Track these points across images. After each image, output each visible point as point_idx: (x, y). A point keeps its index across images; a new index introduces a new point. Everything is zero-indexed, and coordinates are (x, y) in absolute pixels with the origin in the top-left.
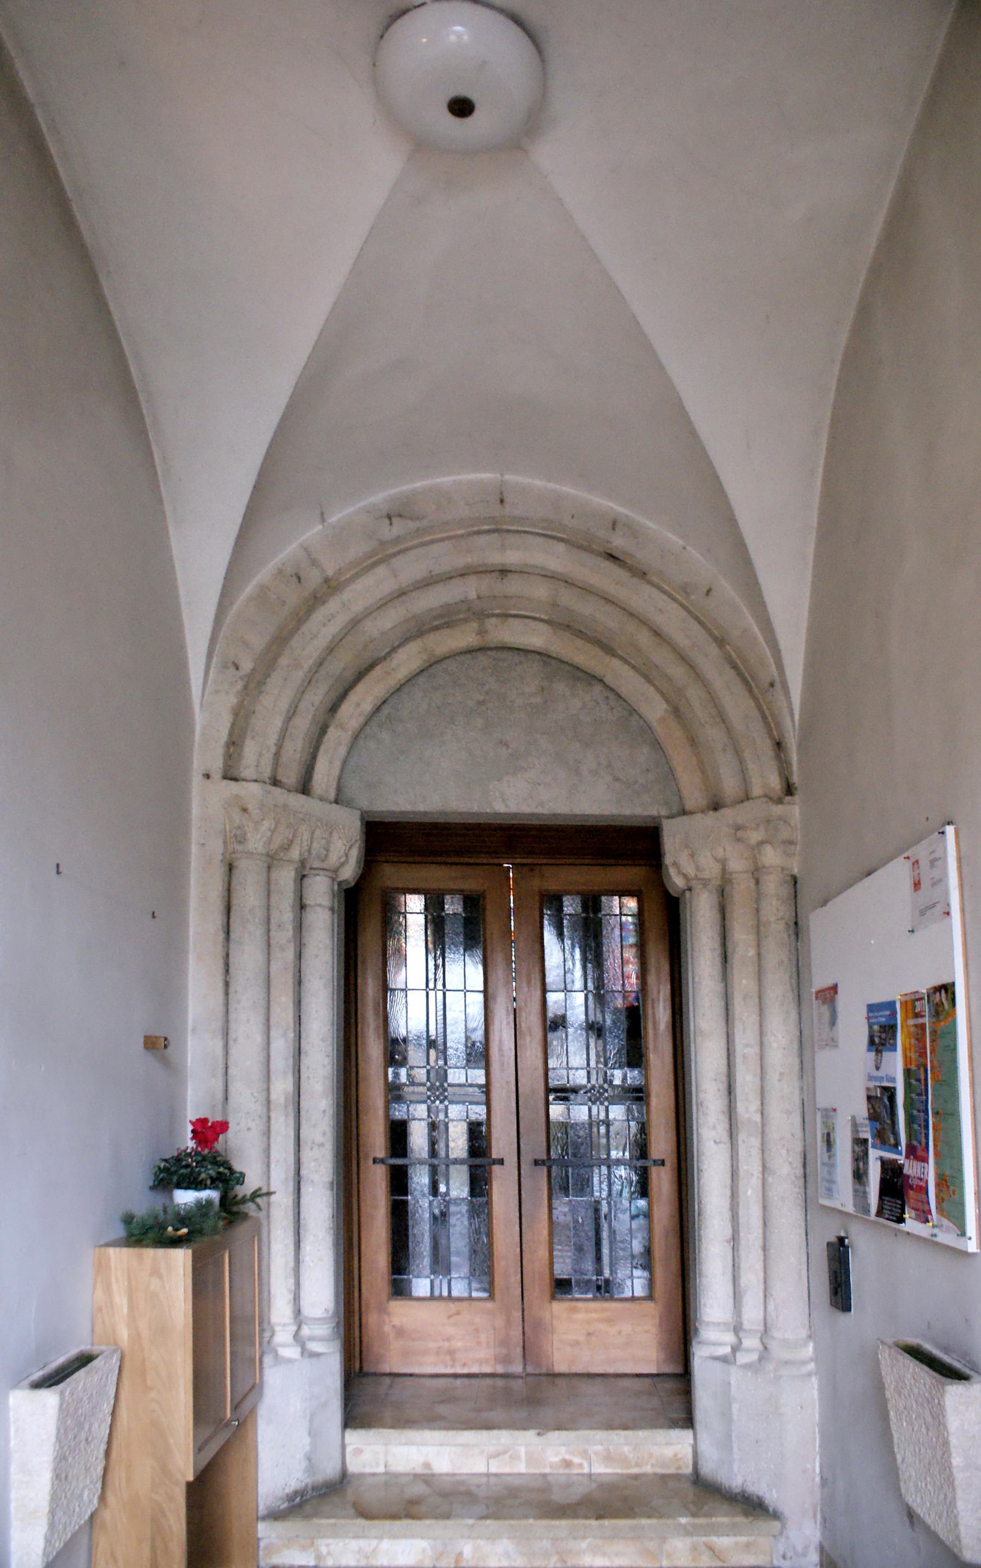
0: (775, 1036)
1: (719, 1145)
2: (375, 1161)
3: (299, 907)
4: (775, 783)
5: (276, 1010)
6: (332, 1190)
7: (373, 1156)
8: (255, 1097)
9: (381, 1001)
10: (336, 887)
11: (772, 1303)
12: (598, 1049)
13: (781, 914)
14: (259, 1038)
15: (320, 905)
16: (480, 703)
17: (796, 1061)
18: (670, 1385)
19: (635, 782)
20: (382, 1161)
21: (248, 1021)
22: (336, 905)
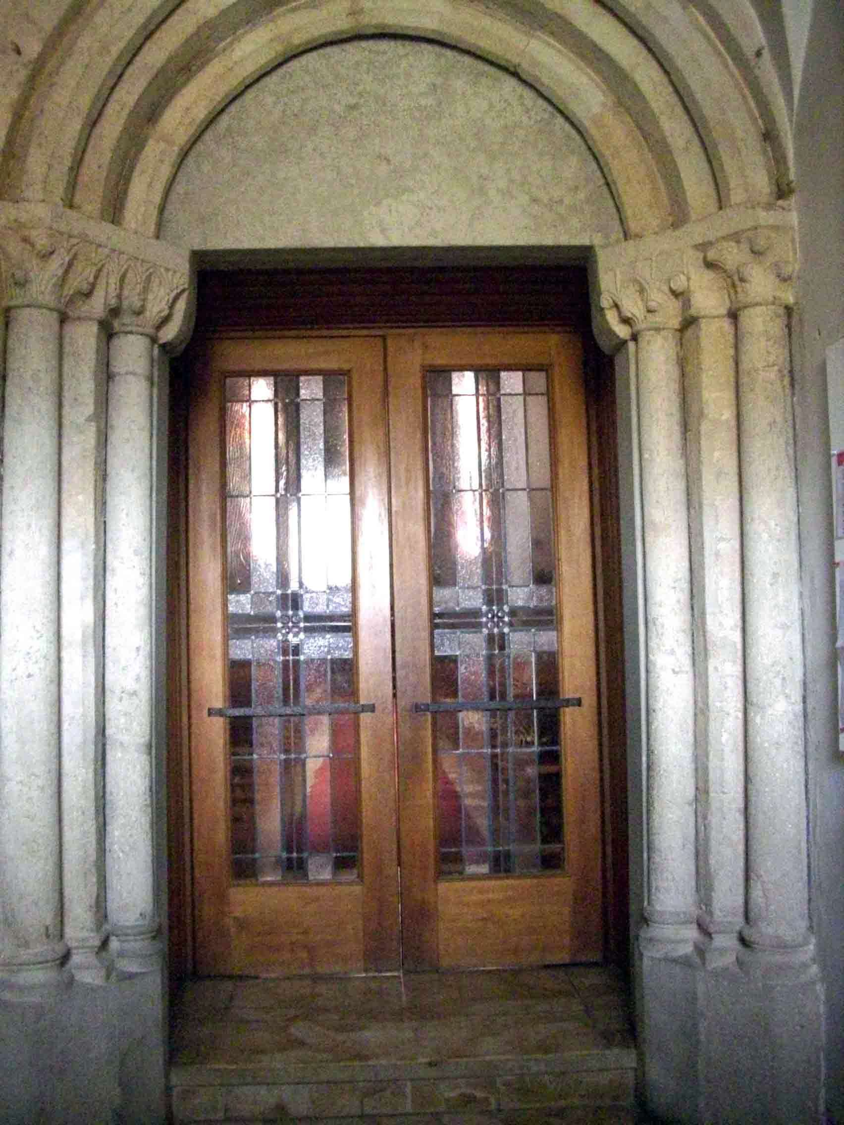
0: (766, 523)
1: (679, 676)
2: (211, 712)
3: (105, 376)
4: (762, 182)
5: (69, 511)
6: (150, 754)
7: (208, 706)
8: (38, 632)
9: (218, 511)
10: (156, 351)
11: (759, 886)
12: (787, 416)
13: (772, 359)
14: (44, 551)
15: (134, 374)
16: (353, 107)
17: (795, 557)
18: (593, 978)
19: (561, 201)
20: (220, 713)
21: (29, 526)
22: (156, 374)
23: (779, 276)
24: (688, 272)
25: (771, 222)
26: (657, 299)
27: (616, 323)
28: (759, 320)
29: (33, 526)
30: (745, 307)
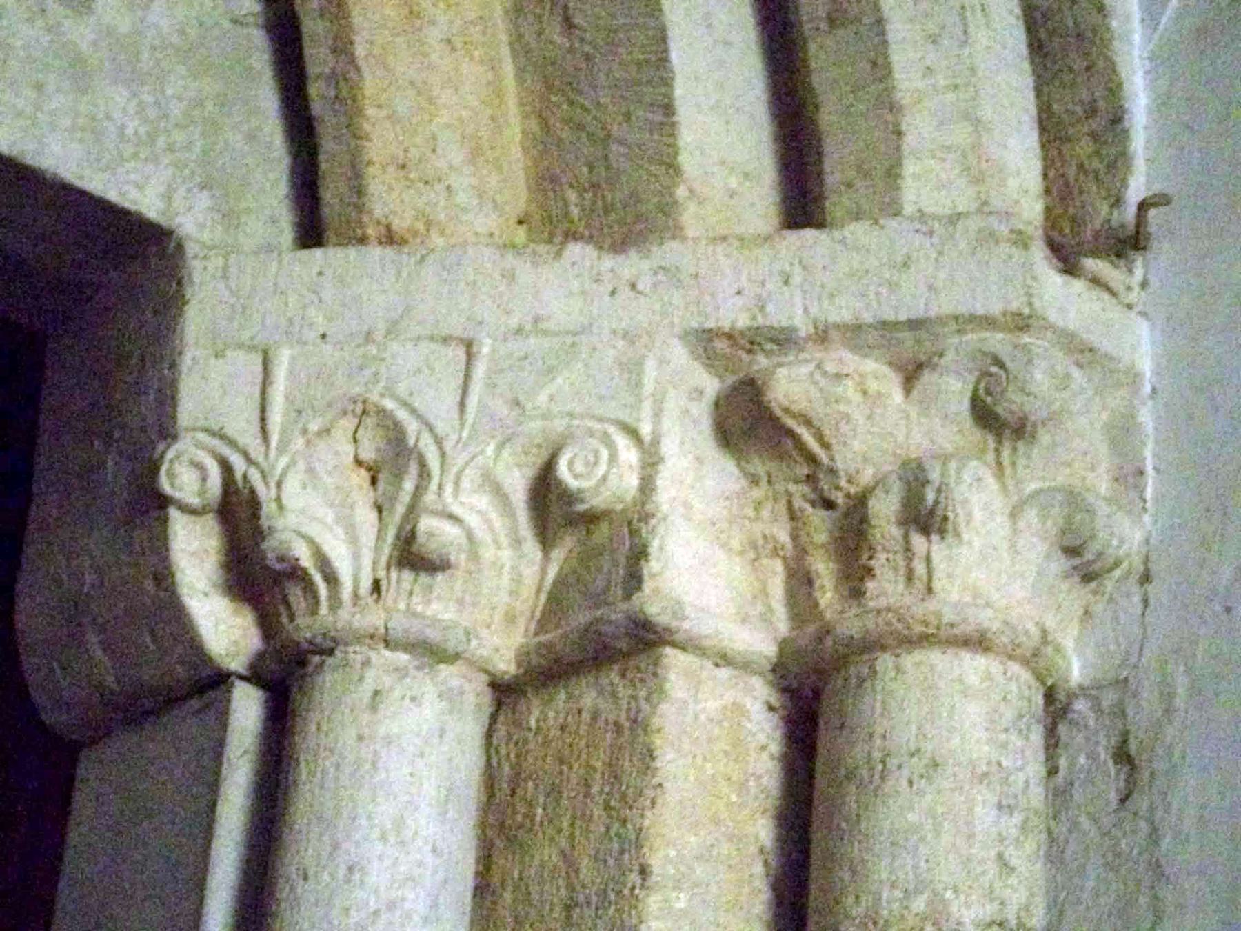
23: (1072, 551)
24: (656, 442)
25: (1072, 322)
26: (473, 521)
27: (202, 585)
28: (973, 712)
29: (1025, 720)
30: (924, 640)
